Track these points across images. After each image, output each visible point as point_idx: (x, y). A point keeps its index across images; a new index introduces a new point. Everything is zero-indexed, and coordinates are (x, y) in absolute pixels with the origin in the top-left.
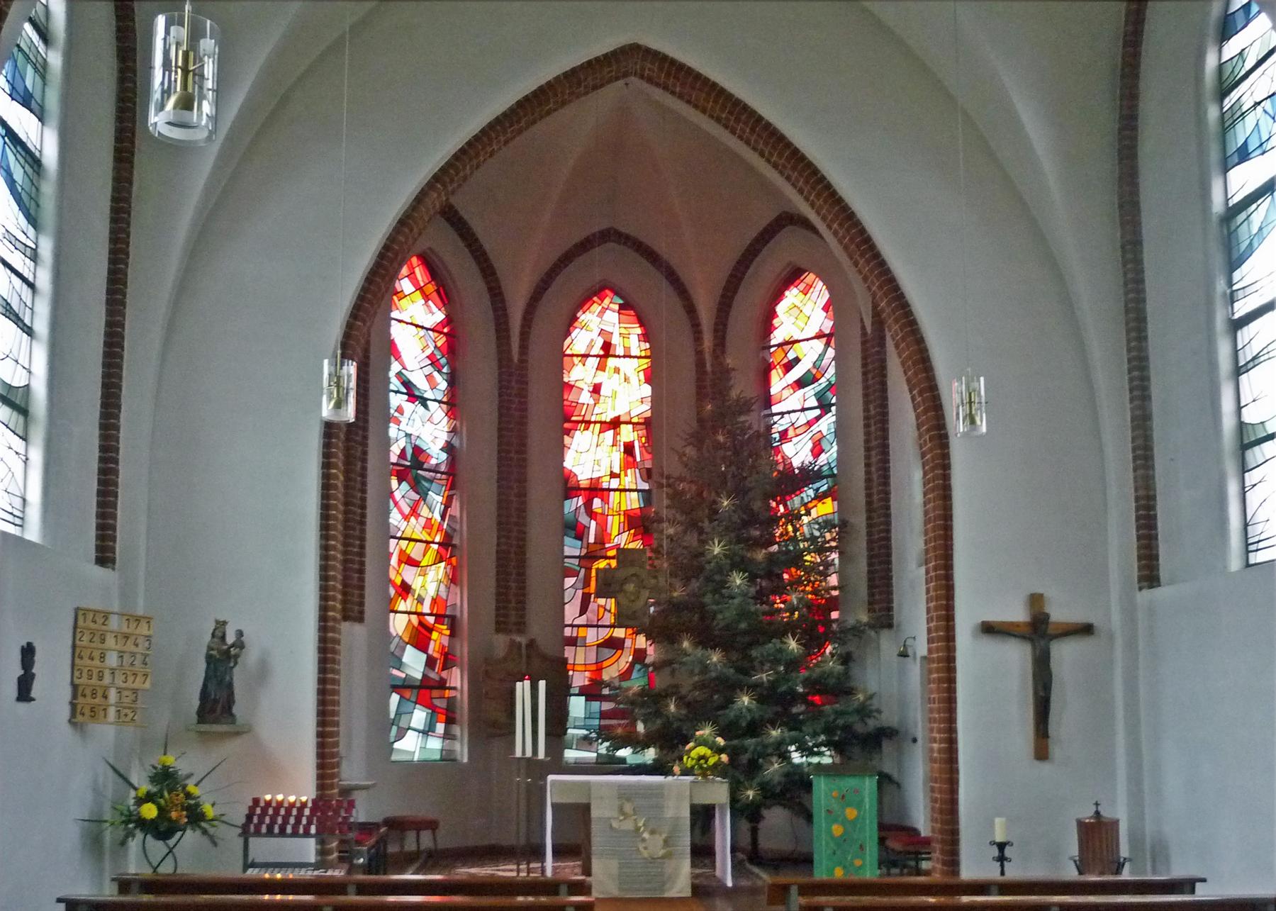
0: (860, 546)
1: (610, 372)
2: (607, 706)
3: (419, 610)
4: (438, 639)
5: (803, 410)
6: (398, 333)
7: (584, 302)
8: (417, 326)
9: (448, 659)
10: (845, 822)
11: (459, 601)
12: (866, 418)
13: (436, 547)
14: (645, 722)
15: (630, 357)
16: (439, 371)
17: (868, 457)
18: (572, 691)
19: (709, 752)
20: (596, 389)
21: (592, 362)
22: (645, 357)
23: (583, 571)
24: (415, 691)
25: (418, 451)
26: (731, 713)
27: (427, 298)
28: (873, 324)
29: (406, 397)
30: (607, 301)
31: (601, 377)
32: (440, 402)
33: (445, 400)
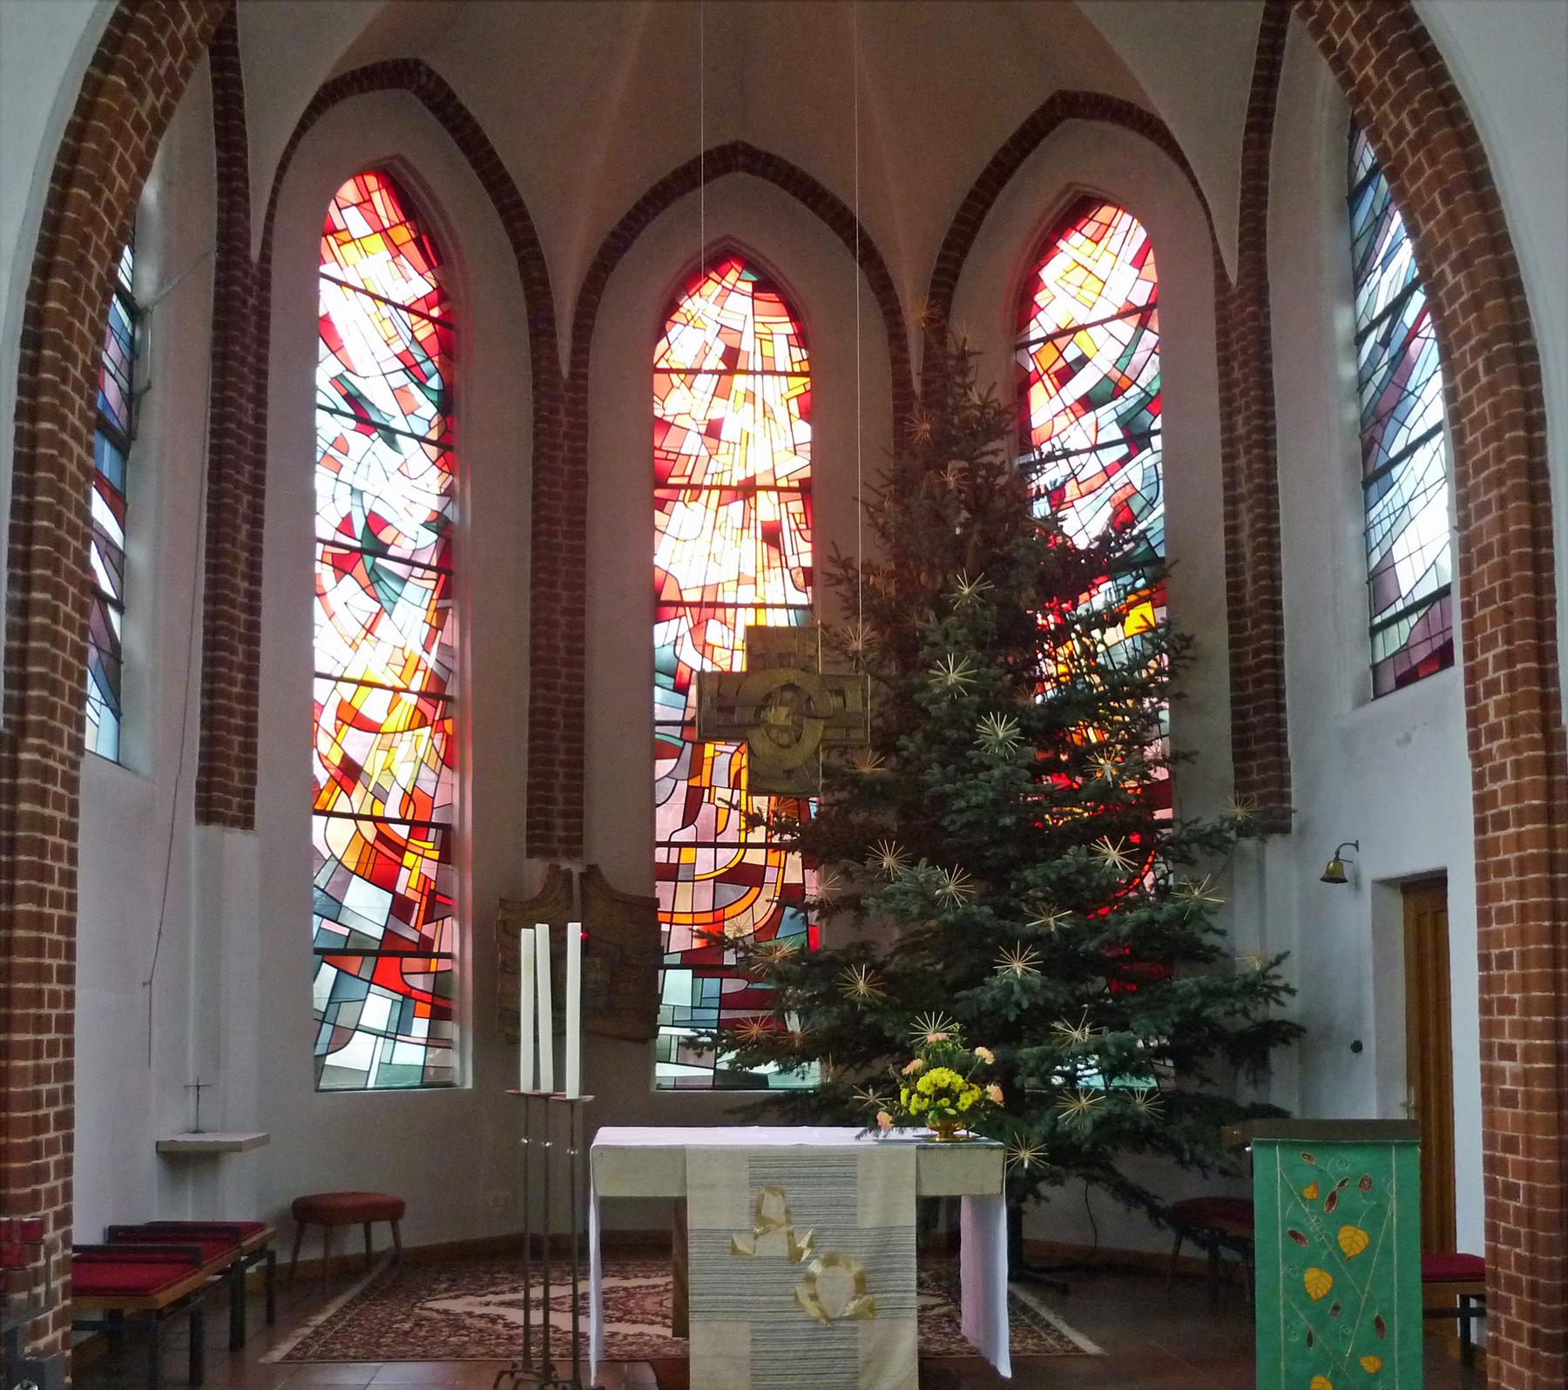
0: (1215, 683)
1: (735, 398)
2: (732, 986)
3: (377, 812)
4: (416, 869)
5: (1095, 448)
6: (330, 300)
7: (690, 281)
8: (375, 297)
9: (435, 902)
10: (1336, 1262)
11: (449, 794)
12: (1229, 443)
13: (413, 699)
14: (804, 1015)
15: (774, 373)
16: (421, 384)
17: (1231, 515)
18: (667, 960)
19: (959, 1080)
20: (713, 430)
21: (705, 383)
22: (802, 374)
23: (689, 746)
24: (371, 960)
25: (375, 523)
26: (985, 995)
27: (396, 250)
28: (1241, 266)
29: (352, 423)
30: (732, 276)
31: (719, 409)
32: (421, 439)
33: (434, 436)
